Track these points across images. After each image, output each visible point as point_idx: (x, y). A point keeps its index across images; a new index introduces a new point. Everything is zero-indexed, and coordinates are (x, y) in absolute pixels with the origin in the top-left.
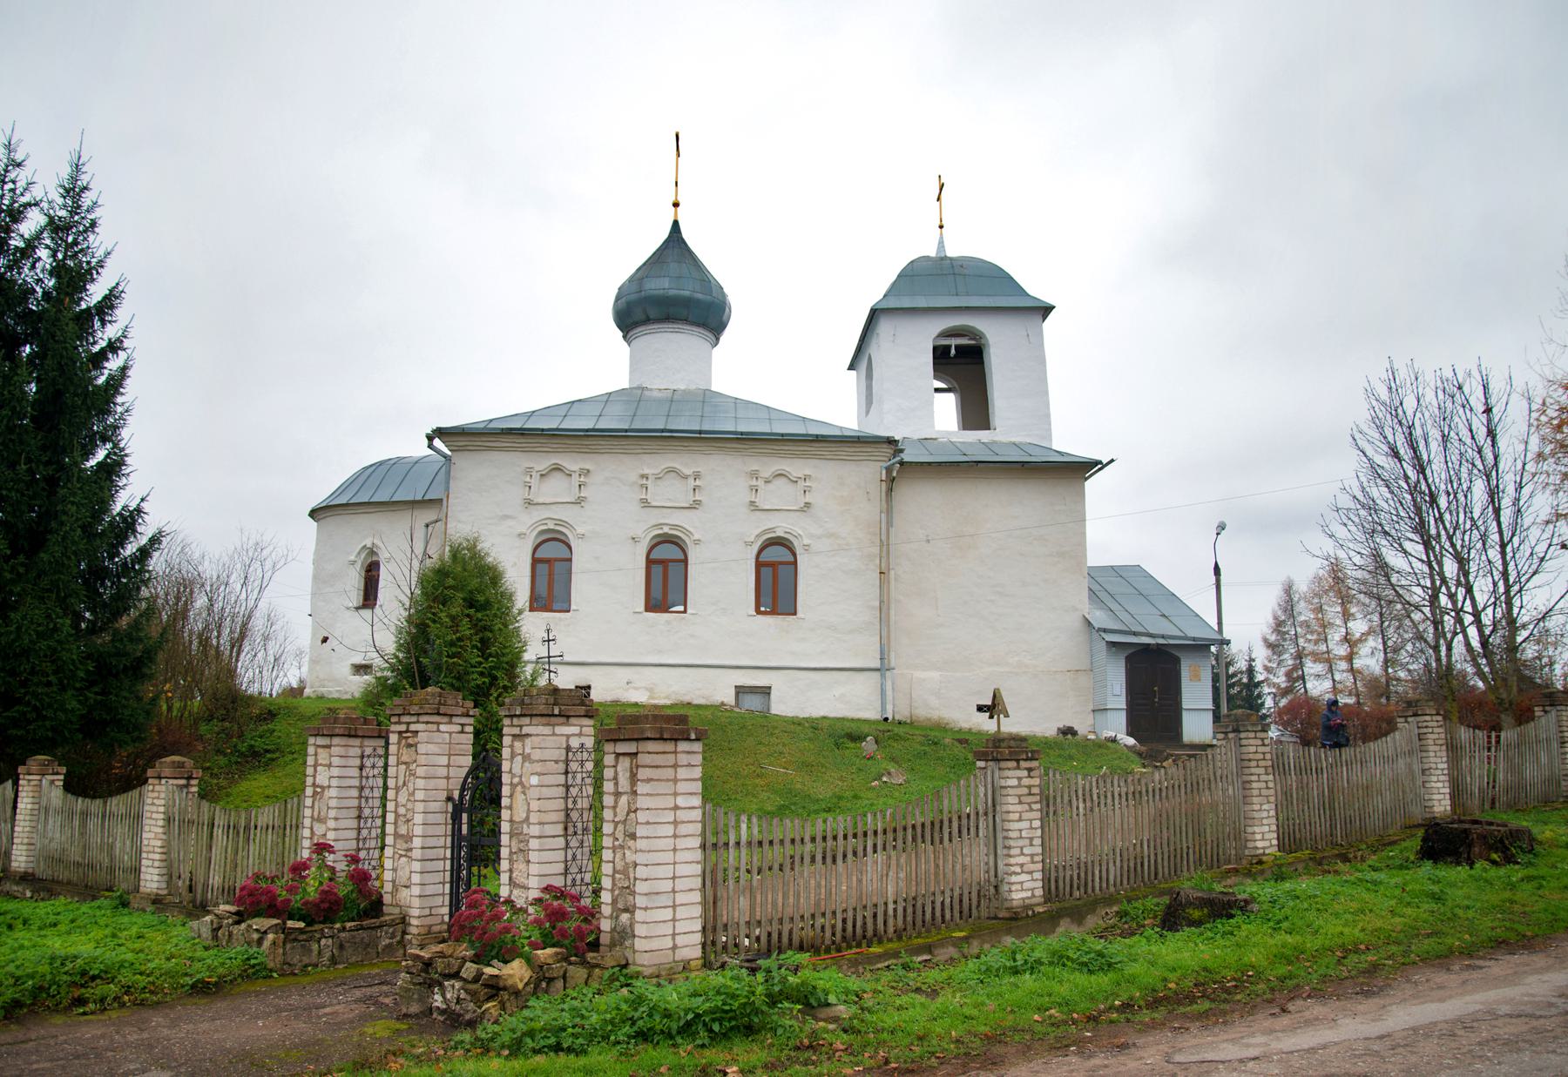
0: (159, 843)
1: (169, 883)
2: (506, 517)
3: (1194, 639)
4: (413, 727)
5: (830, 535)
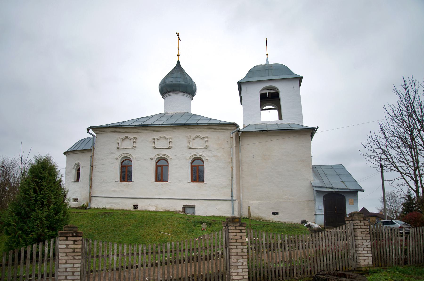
2: (112, 153)
3: (350, 189)
5: (215, 156)
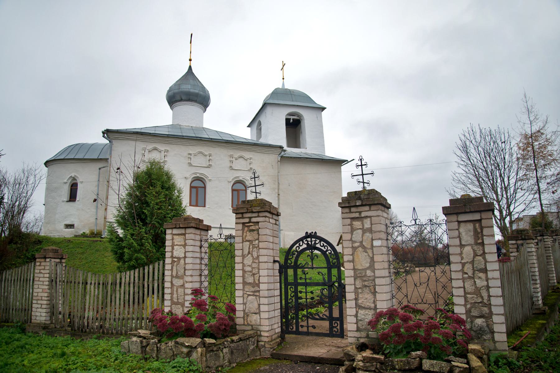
0: (46, 295)
1: (51, 317)
4: (254, 220)
